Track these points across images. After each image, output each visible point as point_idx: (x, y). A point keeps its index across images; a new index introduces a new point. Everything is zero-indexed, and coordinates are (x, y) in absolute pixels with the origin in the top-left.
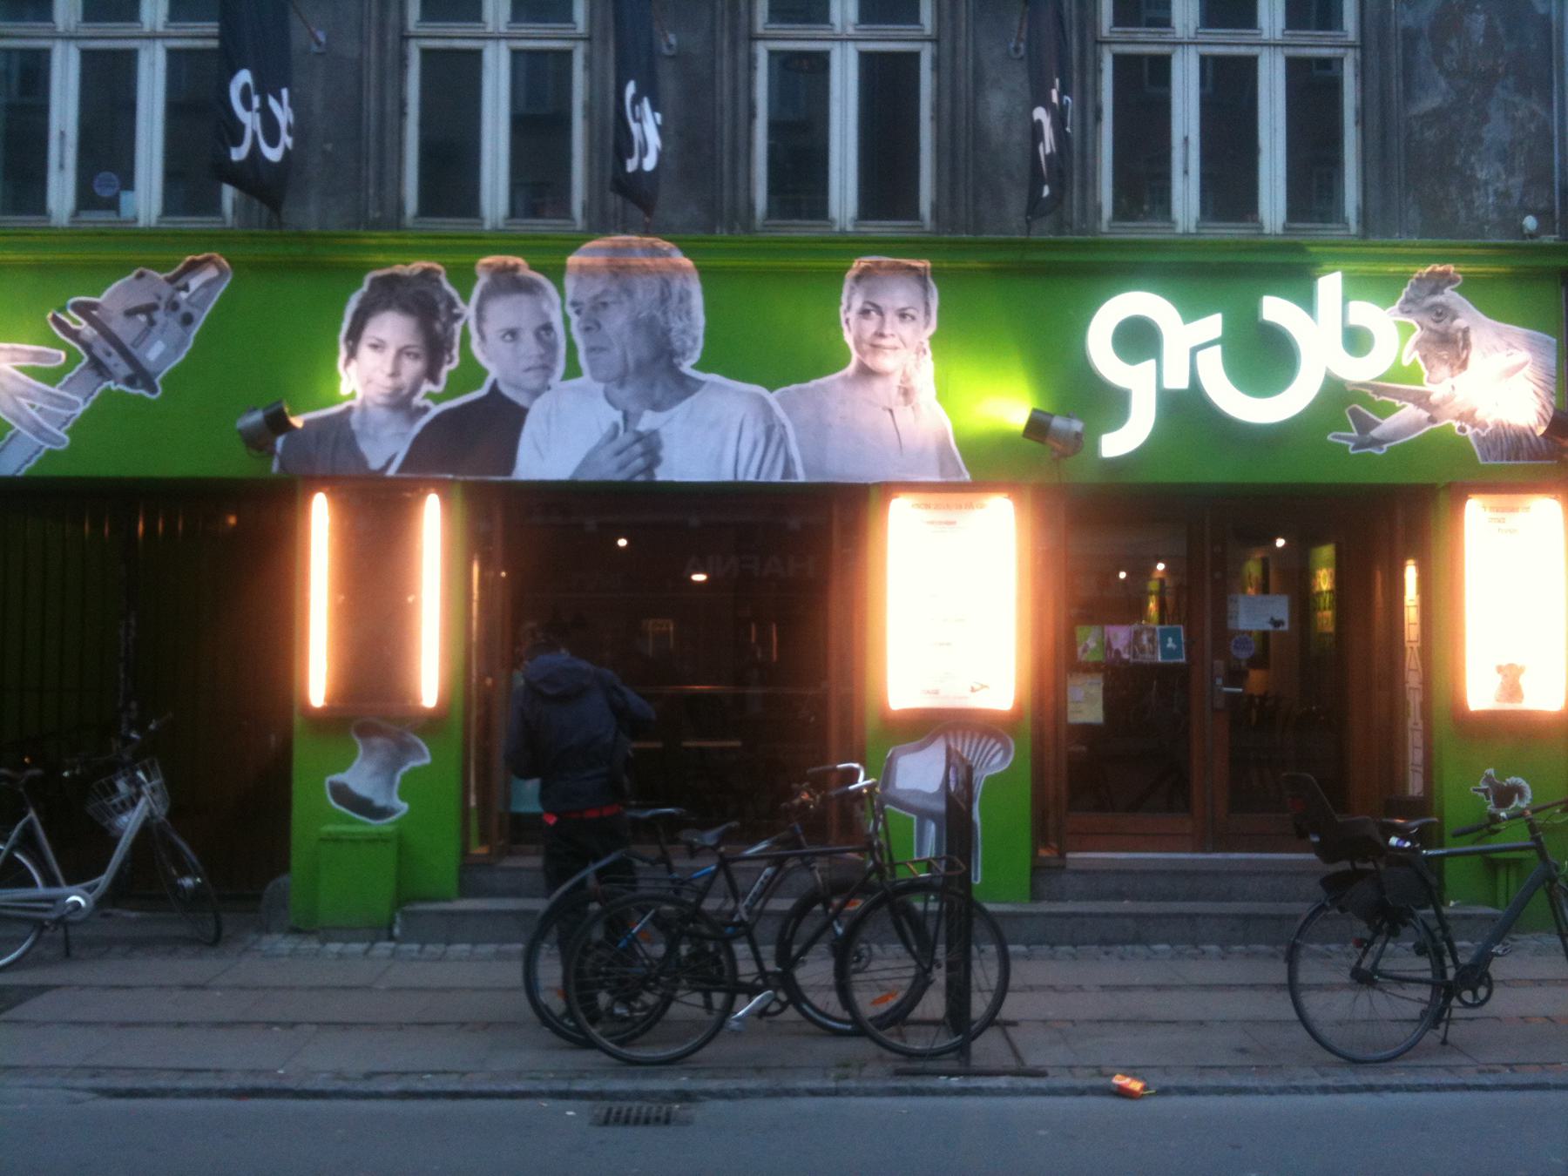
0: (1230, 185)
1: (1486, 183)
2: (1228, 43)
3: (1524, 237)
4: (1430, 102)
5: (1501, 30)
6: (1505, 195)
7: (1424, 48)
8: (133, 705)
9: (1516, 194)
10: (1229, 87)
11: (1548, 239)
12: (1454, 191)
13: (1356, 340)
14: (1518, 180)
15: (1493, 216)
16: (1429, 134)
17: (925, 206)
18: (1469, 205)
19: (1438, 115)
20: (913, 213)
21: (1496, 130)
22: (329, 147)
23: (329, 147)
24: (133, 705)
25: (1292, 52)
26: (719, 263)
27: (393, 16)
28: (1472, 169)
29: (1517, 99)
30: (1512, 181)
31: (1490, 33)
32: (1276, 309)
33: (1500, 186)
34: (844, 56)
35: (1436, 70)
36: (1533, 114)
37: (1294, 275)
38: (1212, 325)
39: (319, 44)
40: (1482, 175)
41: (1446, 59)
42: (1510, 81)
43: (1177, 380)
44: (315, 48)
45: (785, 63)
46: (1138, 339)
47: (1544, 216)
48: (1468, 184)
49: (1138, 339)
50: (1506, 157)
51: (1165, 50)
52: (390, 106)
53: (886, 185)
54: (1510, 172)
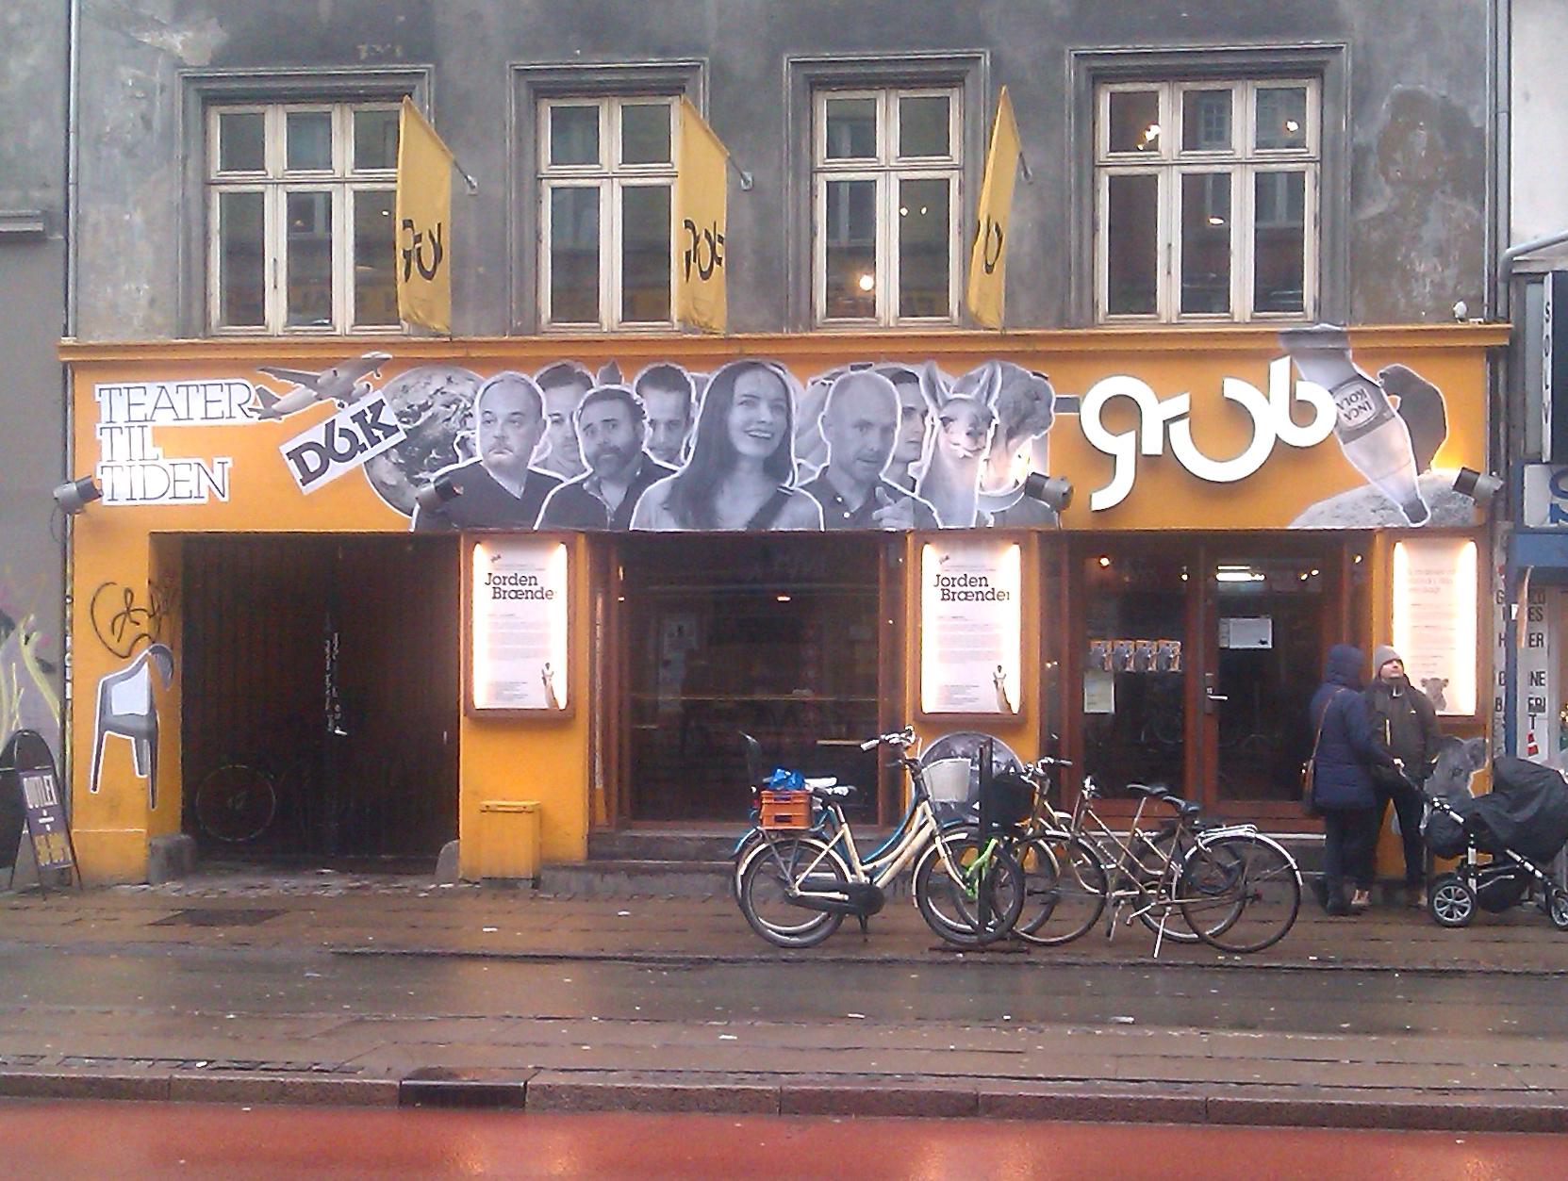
0: (1205, 286)
1: (1424, 275)
2: (1205, 162)
3: (1455, 320)
4: (1374, 209)
5: (1441, 142)
6: (1439, 286)
7: (1373, 161)
8: (337, 707)
9: (1450, 283)
10: (308, 213)
11: (1474, 322)
12: (1394, 283)
13: (1302, 412)
14: (1451, 273)
15: (1429, 304)
16: (1375, 235)
17: (1308, 302)
18: (1408, 294)
19: (1383, 218)
20: (945, 311)
21: (1433, 230)
22: (481, 270)
23: (481, 270)
24: (337, 707)
25: (1260, 168)
26: (202, 356)
27: (529, 164)
28: (1412, 263)
29: (1454, 201)
30: (1447, 273)
31: (1431, 147)
32: (1236, 388)
33: (1437, 278)
34: (887, 185)
35: (1382, 179)
36: (1468, 214)
37: (1249, 354)
38: (1180, 404)
39: (746, 182)
40: (1421, 268)
41: (1392, 169)
42: (1448, 188)
43: (1153, 445)
44: (469, 190)
45: (1193, 186)
46: (1121, 412)
47: (1474, 304)
48: (1408, 277)
49: (1121, 412)
50: (1441, 252)
51: (1225, 169)
52: (529, 235)
53: (1277, 284)
54: (1446, 266)
